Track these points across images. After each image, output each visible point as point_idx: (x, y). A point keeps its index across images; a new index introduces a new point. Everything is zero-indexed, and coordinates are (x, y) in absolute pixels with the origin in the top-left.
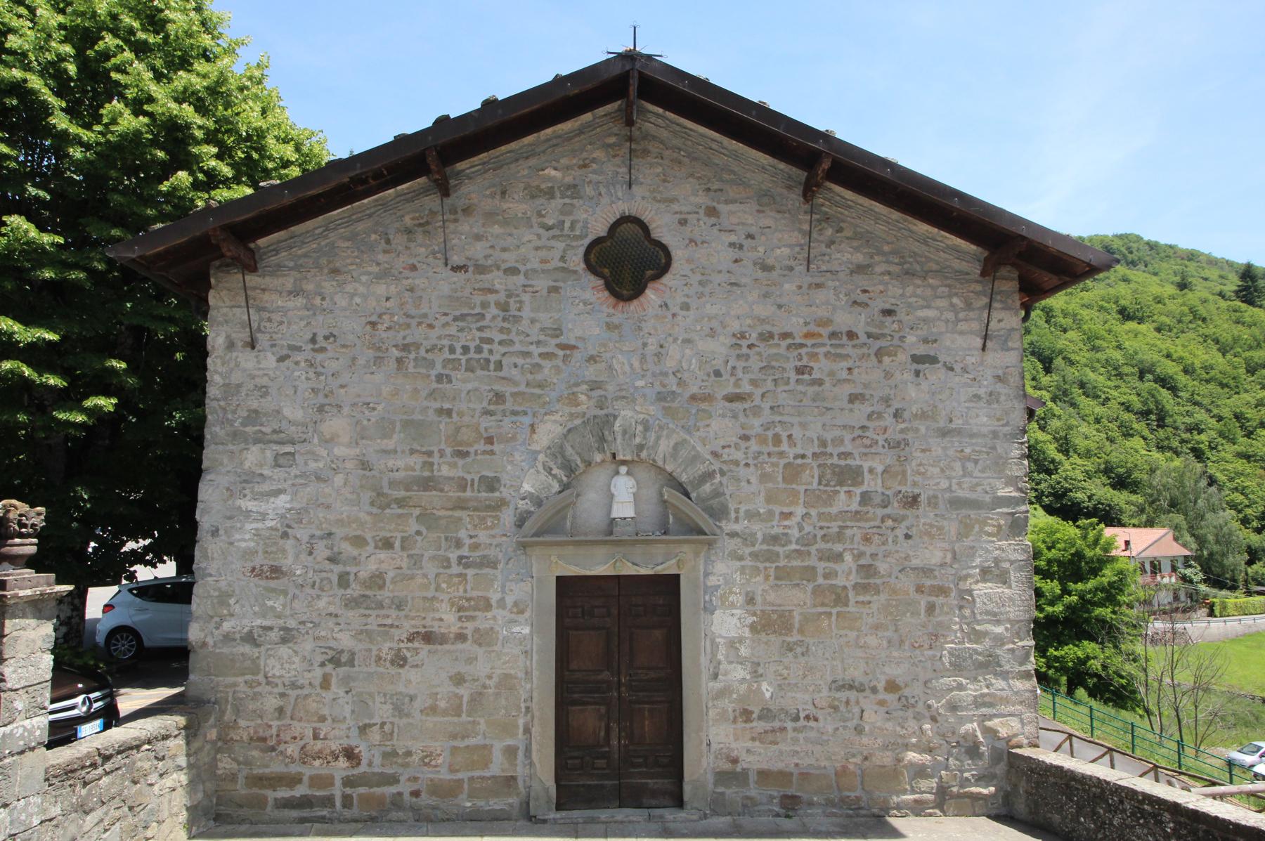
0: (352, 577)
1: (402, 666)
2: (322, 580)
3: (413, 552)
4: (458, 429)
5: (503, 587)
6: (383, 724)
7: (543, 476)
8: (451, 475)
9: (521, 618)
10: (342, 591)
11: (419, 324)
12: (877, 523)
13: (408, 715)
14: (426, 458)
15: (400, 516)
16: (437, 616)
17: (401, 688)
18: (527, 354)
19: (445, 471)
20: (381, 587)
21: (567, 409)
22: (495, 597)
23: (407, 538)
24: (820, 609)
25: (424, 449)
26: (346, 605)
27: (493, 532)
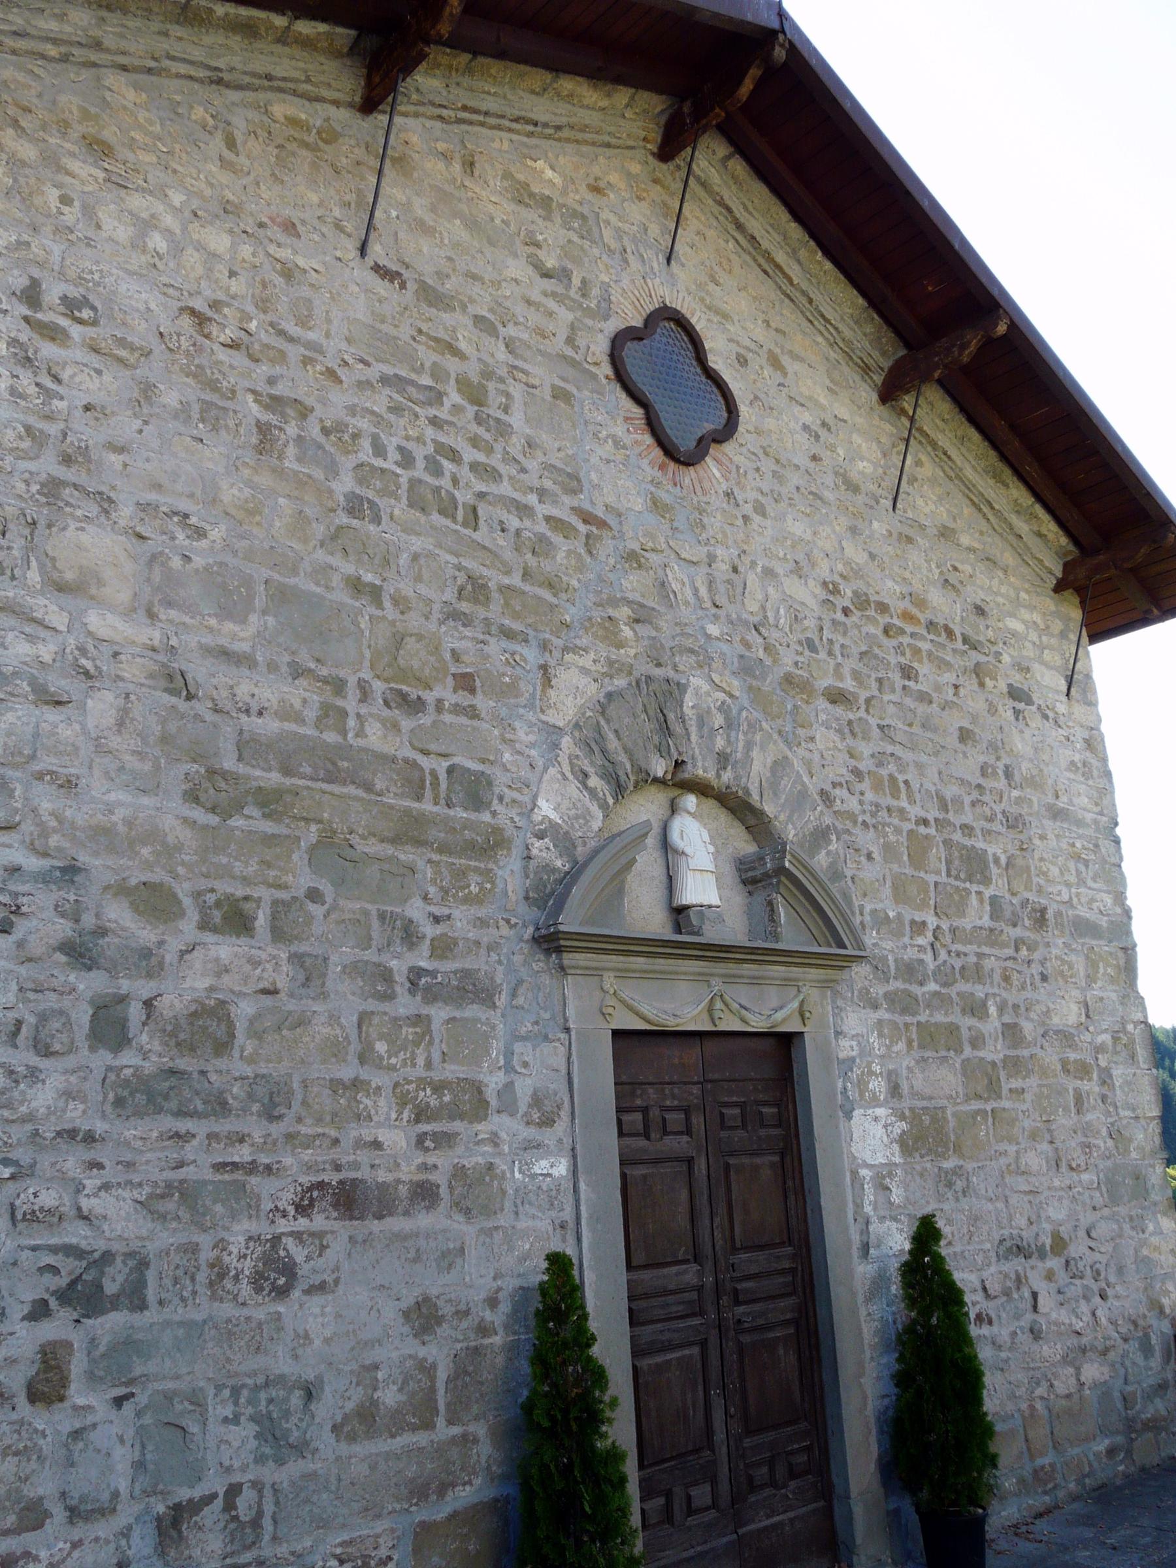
0: (135, 1012)
1: (282, 1293)
2: (43, 1018)
3: (304, 948)
4: (399, 640)
5: (509, 1054)
6: (234, 1491)
7: (573, 788)
8: (388, 749)
9: (549, 1136)
10: (103, 1058)
11: (306, 361)
12: (1010, 952)
13: (301, 1449)
14: (328, 695)
15: (269, 840)
16: (367, 1133)
17: (283, 1366)
18: (524, 510)
19: (375, 737)
20: (223, 1047)
21: (604, 650)
22: (494, 1082)
23: (286, 905)
24: (976, 1105)
25: (324, 672)
26: (119, 1102)
27: (482, 912)
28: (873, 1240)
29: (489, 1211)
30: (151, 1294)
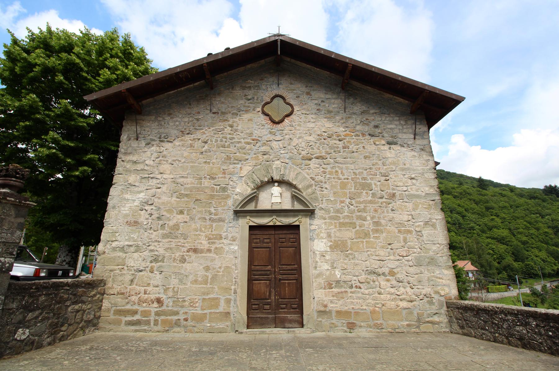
1: (184, 263)
6: (175, 287)
15: (187, 201)
16: (200, 241)
20: (178, 230)
22: (224, 235)
30: (165, 261)
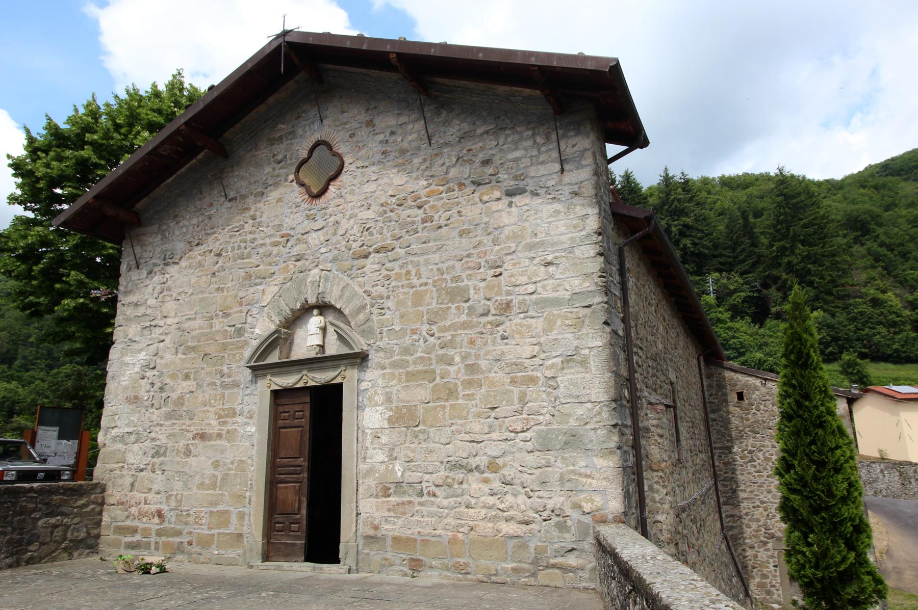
1: (188, 456)
6: (177, 495)
9: (251, 421)
16: (208, 422)
28: (368, 455)
29: (234, 441)
